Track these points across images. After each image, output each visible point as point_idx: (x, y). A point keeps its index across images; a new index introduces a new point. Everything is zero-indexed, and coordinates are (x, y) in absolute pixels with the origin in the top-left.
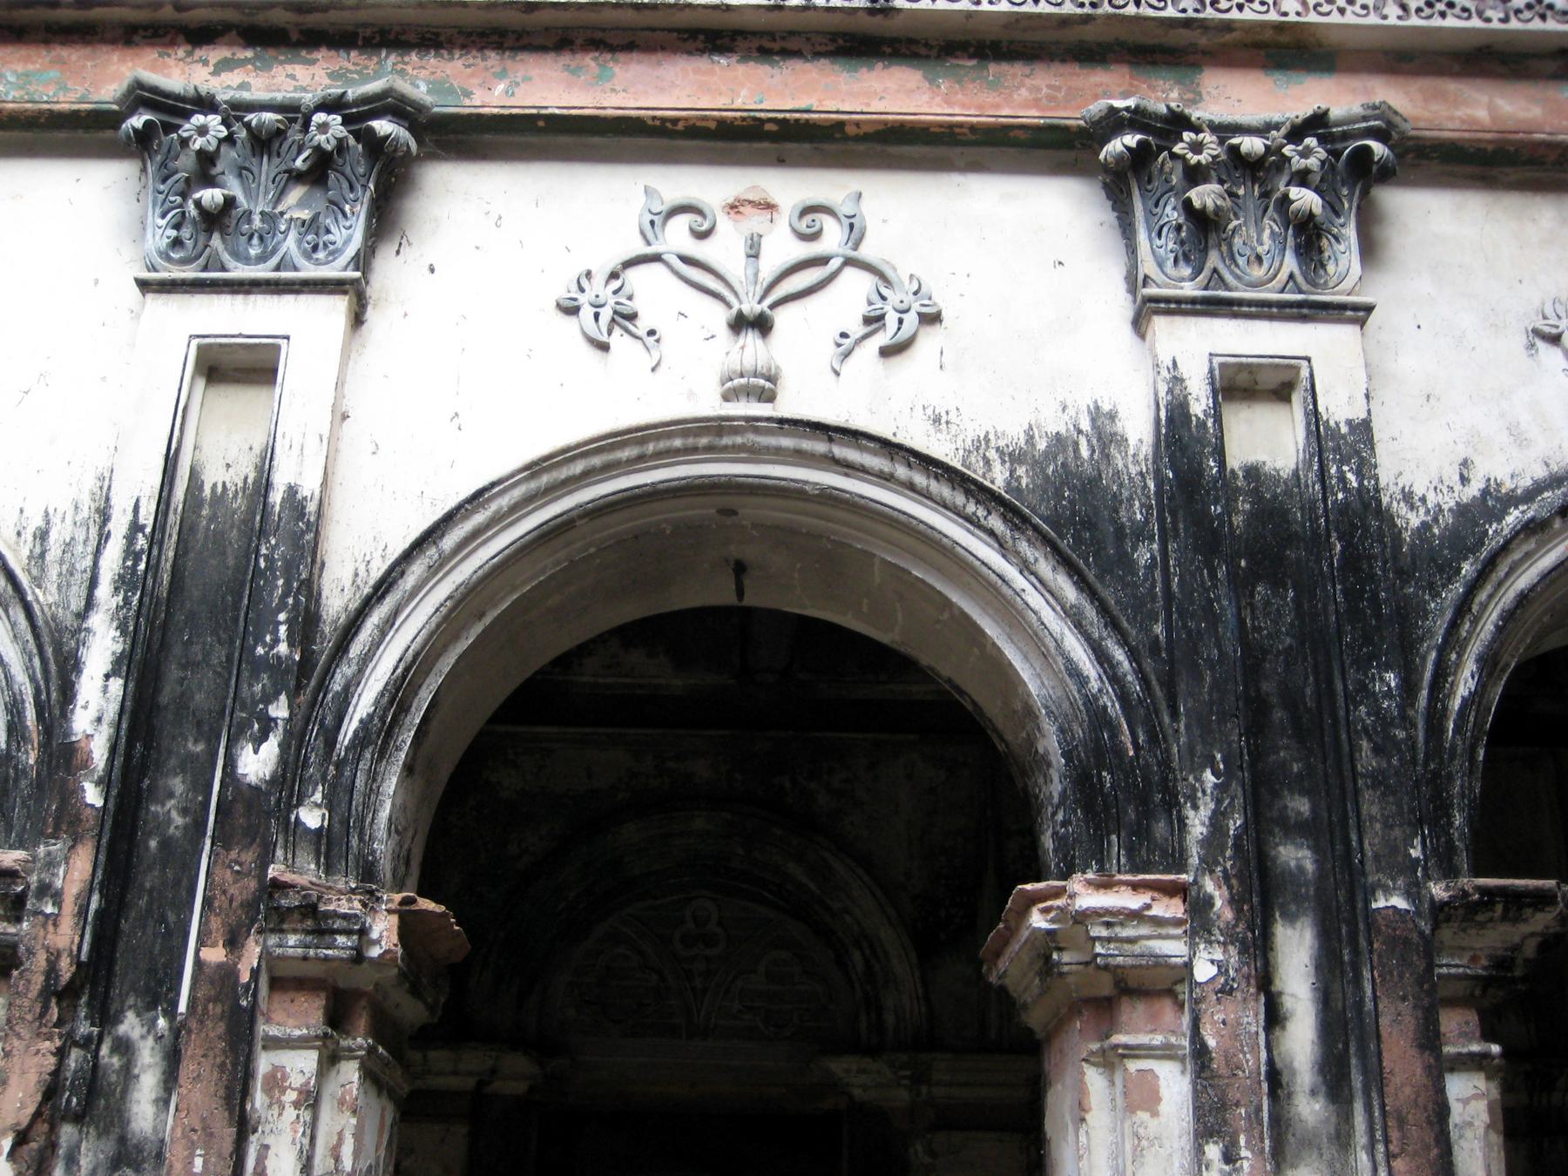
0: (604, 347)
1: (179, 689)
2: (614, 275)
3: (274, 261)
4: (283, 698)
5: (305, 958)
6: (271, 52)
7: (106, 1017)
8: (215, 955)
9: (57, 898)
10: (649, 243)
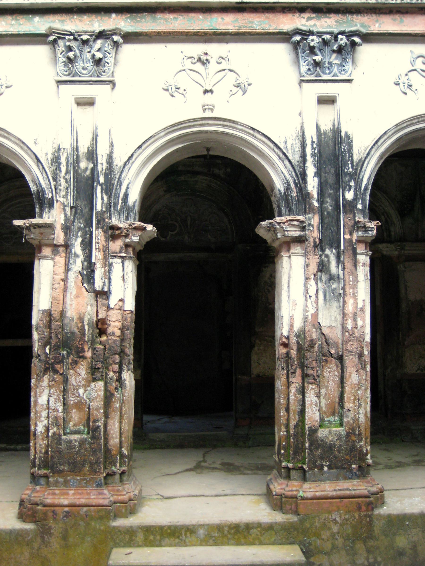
0: (406, 94)
1: (325, 178)
2: (406, 75)
3: (332, 74)
4: (352, 181)
5: (363, 236)
6: (320, 15)
7: (323, 250)
8: (348, 237)
9: (313, 226)
10: (413, 66)
